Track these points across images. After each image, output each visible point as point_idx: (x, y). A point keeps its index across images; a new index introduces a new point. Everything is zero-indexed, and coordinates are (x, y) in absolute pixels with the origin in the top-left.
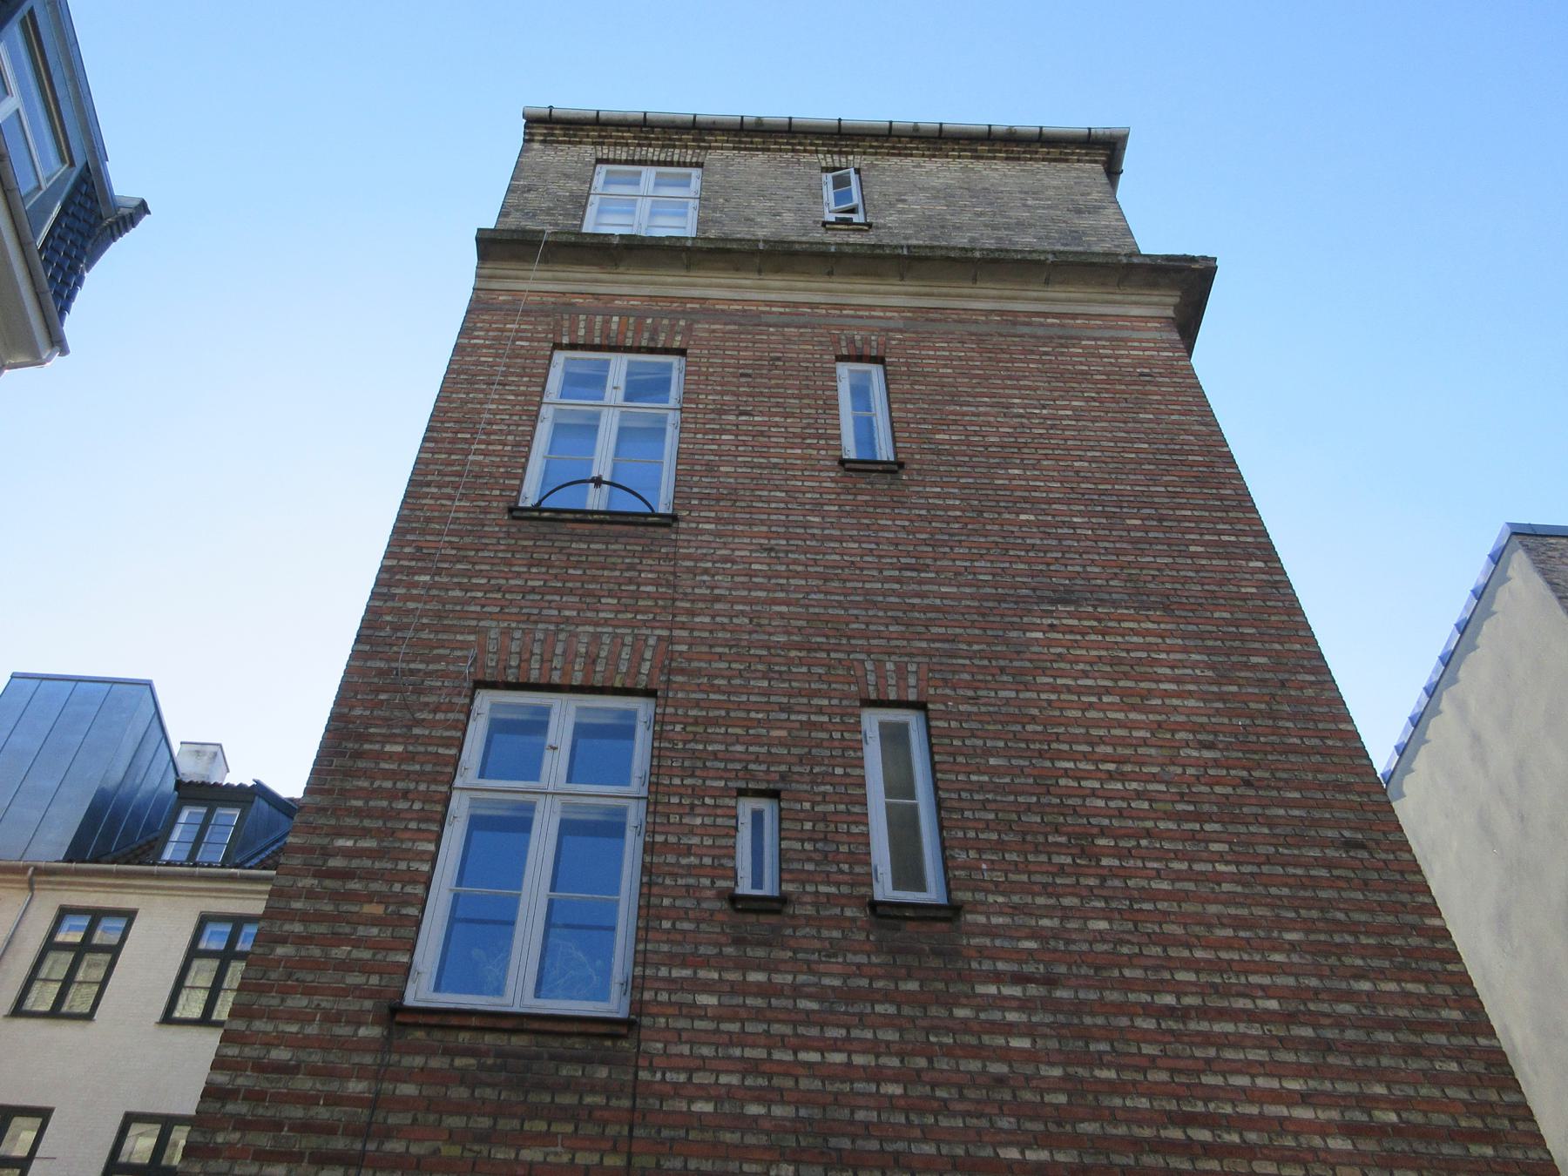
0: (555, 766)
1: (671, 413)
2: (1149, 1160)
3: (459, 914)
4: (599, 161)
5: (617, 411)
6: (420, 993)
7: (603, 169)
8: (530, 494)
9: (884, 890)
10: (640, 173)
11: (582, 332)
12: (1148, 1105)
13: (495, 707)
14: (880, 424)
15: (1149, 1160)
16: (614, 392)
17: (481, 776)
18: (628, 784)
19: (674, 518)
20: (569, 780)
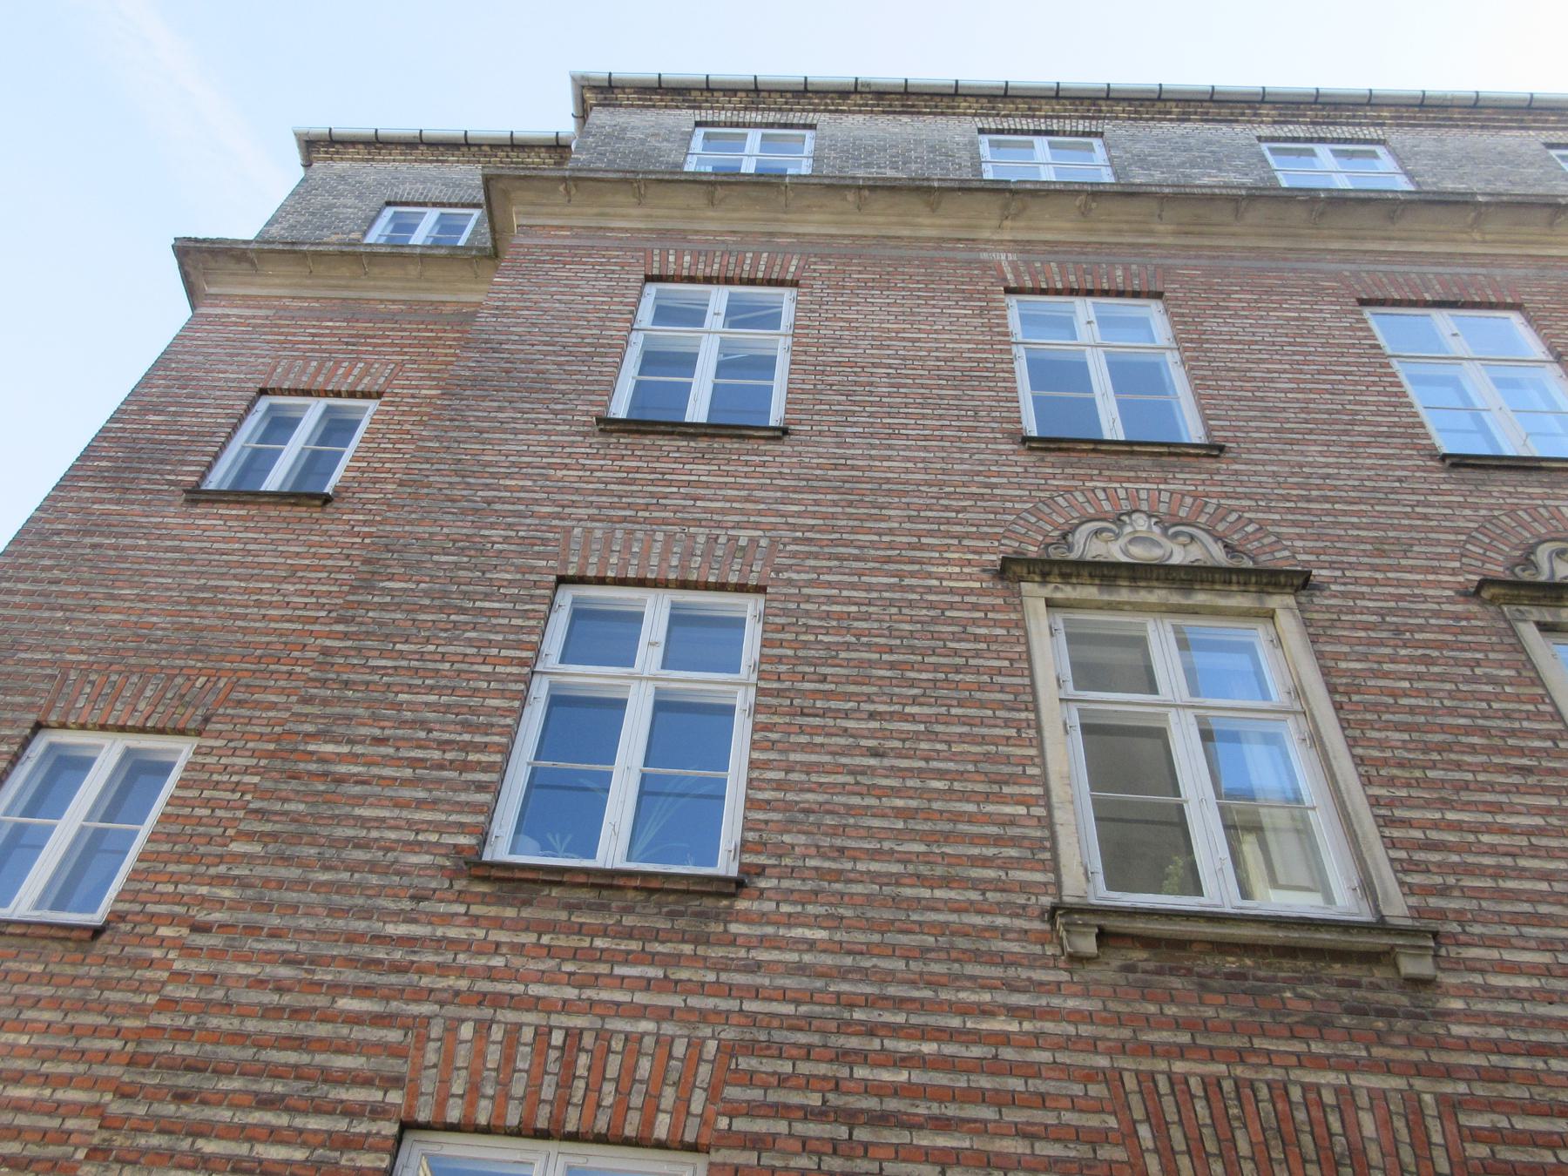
0: (649, 656)
1: (782, 339)
2: (1505, 1153)
3: (536, 782)
4: (698, 124)
5: (717, 337)
6: (500, 850)
7: (701, 132)
8: (620, 408)
9: (1082, 871)
10: (745, 136)
11: (746, 268)
12: (1514, 1120)
13: (575, 601)
14: (1318, 936)
15: (1505, 1153)
16: (715, 320)
17: (562, 661)
18: (737, 671)
19: (785, 431)
20: (664, 667)
